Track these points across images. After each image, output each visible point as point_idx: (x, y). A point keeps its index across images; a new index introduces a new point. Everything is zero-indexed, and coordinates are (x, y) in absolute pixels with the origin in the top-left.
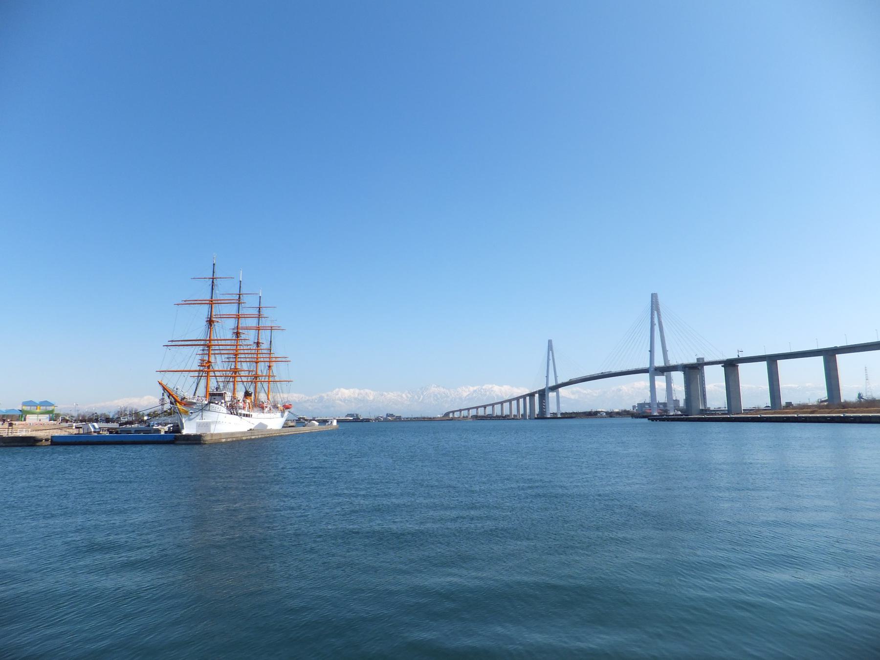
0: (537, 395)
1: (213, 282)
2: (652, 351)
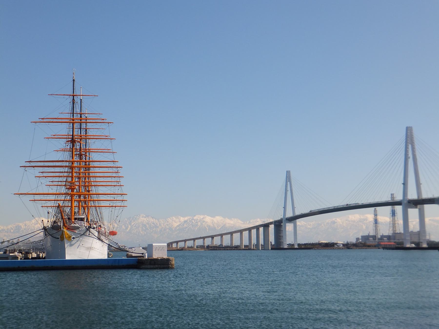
1: (73, 99)
2: (405, 184)
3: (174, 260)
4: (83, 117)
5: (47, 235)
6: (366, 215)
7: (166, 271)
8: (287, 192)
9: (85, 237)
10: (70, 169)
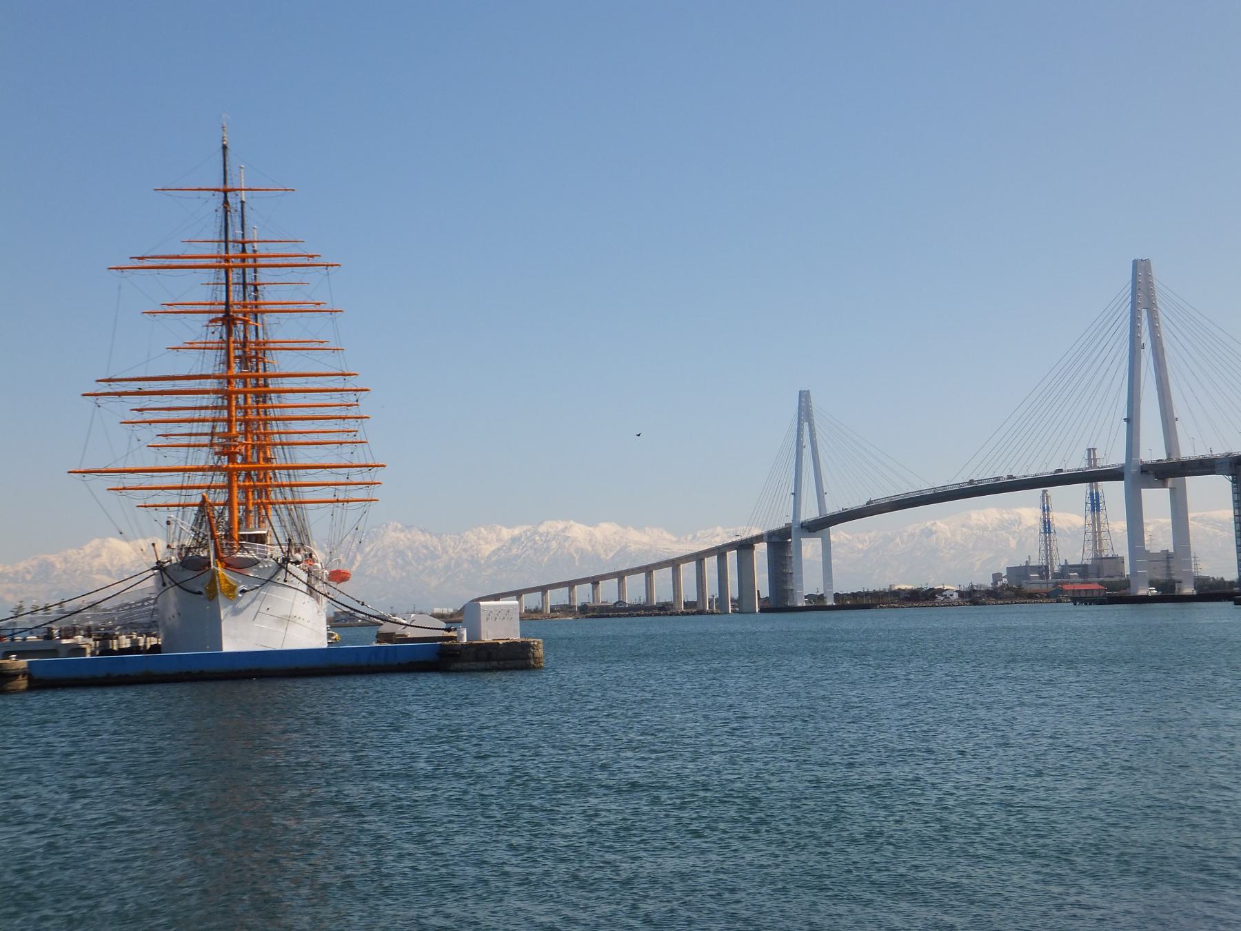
1: (226, 202)
2: (1132, 421)
3: (541, 646)
4: (249, 251)
5: (168, 585)
6: (1018, 510)
7: (518, 675)
8: (802, 450)
9: (274, 587)
10: (223, 398)
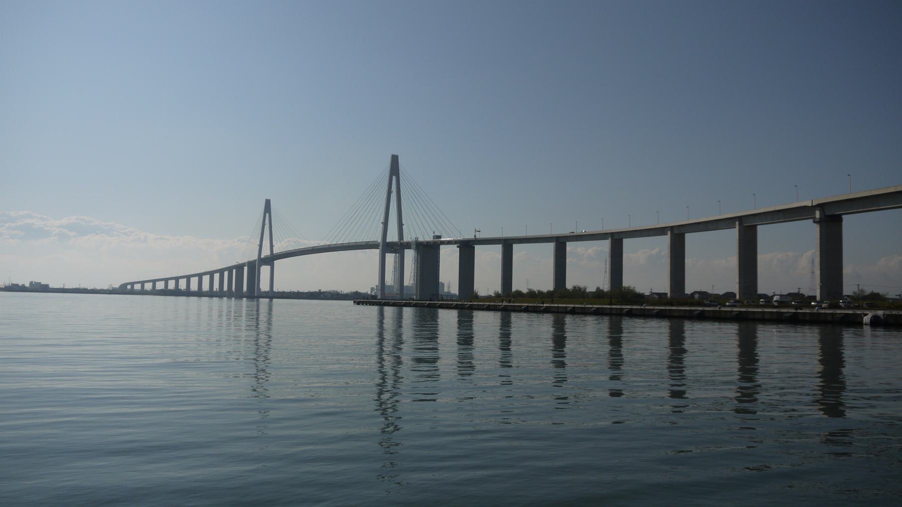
0: (246, 269)
2: (386, 224)
